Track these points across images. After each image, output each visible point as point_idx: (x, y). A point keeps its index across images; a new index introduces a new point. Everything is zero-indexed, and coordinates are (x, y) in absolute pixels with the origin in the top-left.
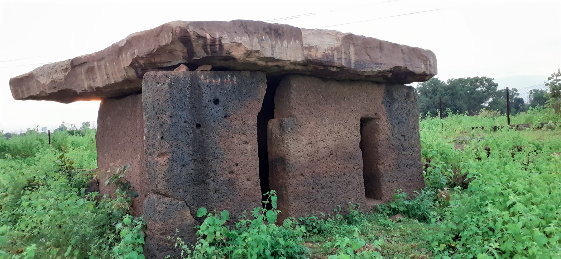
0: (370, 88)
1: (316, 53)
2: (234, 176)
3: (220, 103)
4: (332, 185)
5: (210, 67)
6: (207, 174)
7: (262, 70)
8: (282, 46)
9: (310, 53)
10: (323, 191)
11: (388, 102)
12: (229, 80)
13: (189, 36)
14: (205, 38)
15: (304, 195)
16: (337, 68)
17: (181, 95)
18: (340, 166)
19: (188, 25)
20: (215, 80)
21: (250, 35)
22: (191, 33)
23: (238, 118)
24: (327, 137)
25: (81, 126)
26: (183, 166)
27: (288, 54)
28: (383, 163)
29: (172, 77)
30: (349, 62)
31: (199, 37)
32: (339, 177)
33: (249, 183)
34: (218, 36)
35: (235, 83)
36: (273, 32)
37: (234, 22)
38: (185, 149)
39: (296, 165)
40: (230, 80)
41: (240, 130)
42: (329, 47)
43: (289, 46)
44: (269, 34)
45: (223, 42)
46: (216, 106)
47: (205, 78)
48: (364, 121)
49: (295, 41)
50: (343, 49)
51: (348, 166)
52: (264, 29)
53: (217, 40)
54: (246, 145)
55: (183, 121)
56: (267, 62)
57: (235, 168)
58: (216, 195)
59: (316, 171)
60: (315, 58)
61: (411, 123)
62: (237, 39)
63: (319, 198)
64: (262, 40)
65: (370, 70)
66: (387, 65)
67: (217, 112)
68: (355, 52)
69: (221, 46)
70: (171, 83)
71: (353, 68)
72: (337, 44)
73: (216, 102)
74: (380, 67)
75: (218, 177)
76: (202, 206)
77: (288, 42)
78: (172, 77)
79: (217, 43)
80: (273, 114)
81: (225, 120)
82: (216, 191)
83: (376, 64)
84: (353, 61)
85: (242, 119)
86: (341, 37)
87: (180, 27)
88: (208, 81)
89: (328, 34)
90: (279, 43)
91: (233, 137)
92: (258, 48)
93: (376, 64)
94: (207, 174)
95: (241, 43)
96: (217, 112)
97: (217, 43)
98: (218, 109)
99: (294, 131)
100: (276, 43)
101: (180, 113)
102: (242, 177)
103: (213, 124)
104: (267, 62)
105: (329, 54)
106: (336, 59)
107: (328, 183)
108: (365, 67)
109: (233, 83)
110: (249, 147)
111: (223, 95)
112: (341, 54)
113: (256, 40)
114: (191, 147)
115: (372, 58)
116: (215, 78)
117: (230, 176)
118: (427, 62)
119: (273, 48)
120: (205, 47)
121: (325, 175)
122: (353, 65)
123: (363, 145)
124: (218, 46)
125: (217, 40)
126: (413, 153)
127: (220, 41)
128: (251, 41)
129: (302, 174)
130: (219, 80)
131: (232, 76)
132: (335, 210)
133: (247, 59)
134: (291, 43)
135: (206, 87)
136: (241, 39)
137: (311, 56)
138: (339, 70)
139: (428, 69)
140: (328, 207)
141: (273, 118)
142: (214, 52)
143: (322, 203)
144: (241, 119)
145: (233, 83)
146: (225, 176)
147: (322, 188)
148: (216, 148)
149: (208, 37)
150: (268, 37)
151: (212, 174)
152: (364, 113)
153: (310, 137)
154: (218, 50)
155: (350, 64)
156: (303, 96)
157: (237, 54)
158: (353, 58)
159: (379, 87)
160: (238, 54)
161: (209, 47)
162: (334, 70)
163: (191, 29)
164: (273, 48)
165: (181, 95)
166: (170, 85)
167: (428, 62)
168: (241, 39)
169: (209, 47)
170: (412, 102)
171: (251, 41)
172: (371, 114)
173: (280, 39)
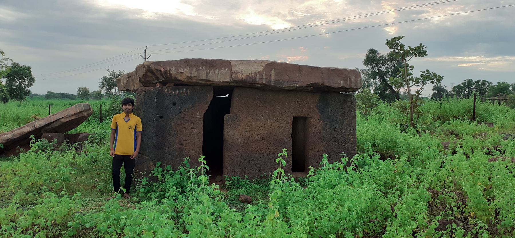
0: (304, 96)
1: (241, 76)
2: (183, 147)
3: (177, 105)
4: (261, 159)
5: (173, 84)
6: (165, 144)
7: (210, 85)
8: (214, 72)
9: (236, 76)
10: (254, 162)
11: (322, 106)
12: (184, 91)
13: (152, 70)
14: (161, 71)
15: (237, 163)
16: (261, 84)
17: (151, 100)
18: (270, 148)
19: (151, 64)
20: (174, 91)
21: (191, 67)
22: (153, 68)
23: (189, 113)
24: (261, 128)
25: (496, 84)
26: (150, 138)
27: (219, 77)
28: (313, 149)
29: (146, 91)
30: (270, 81)
31: (157, 70)
32: (268, 155)
33: (193, 152)
34: (168, 69)
35: (189, 93)
36: (208, 64)
37: (181, 60)
38: (451, 130)
39: (233, 144)
40: (185, 92)
41: (190, 121)
42: (253, 71)
43: (220, 72)
44: (205, 66)
45: (171, 72)
46: (174, 106)
47: (168, 91)
48: (296, 120)
49: (225, 69)
50: (265, 73)
51: (278, 148)
52: (202, 63)
53: (168, 71)
54: (194, 130)
55: (152, 114)
56: (206, 82)
57: (184, 142)
58: (170, 156)
59: (249, 149)
60: (240, 79)
61: (345, 122)
62: (181, 70)
63: (249, 166)
64: (199, 70)
65: (287, 86)
66: (304, 82)
67: (174, 110)
68: (275, 74)
69: (170, 74)
70: (145, 94)
71: (272, 84)
72: (261, 69)
73: (174, 104)
74: (297, 84)
75: (171, 146)
76: (160, 161)
77: (220, 70)
78: (146, 91)
79: (168, 73)
80: (230, 110)
81: (180, 115)
82: (170, 154)
83: (294, 82)
84: (273, 80)
85: (192, 115)
86: (264, 64)
87: (147, 65)
88: (169, 92)
89: (255, 63)
90: (212, 70)
91: (184, 125)
92: (196, 74)
93: (294, 82)
94: (165, 144)
95: (183, 72)
96: (174, 110)
97: (168, 73)
98: (175, 108)
99: (233, 123)
100: (210, 71)
101: (149, 110)
102: (189, 148)
103: (170, 117)
104: (206, 82)
105: (252, 76)
106: (257, 79)
107: (258, 158)
108: (284, 84)
109: (187, 93)
110: (195, 131)
111: (180, 100)
112: (263, 76)
113: (194, 70)
114: (155, 129)
115: (290, 77)
116: (175, 90)
117: (180, 146)
118: (347, 79)
119: (207, 74)
120: (162, 74)
121: (256, 152)
122: (83, 108)
123: (294, 135)
124: (169, 75)
125: (168, 71)
126: (346, 144)
127: (170, 72)
128: (191, 71)
129: (237, 150)
130: (177, 92)
131: (187, 90)
132: (261, 175)
133: (190, 81)
134: (222, 70)
135: (168, 95)
136: (183, 70)
137: (237, 77)
138: (263, 86)
139: (348, 83)
140: (256, 173)
141: (229, 113)
142: (167, 77)
143: (251, 170)
144: (191, 114)
145: (187, 93)
146: (176, 146)
147: (253, 160)
148: (172, 130)
149: (162, 69)
150: (204, 68)
151: (167, 144)
152: (297, 113)
153: (246, 128)
154: (169, 76)
155: (271, 82)
156: (243, 101)
157: (182, 78)
158: (273, 78)
159: (314, 95)
160: (182, 78)
161: (164, 75)
162: (259, 86)
163: (152, 66)
164: (207, 74)
165: (151, 100)
166: (145, 95)
167: (348, 79)
168: (183, 70)
169: (164, 75)
170: (349, 107)
171: (191, 71)
172: (304, 114)
173: (213, 68)
